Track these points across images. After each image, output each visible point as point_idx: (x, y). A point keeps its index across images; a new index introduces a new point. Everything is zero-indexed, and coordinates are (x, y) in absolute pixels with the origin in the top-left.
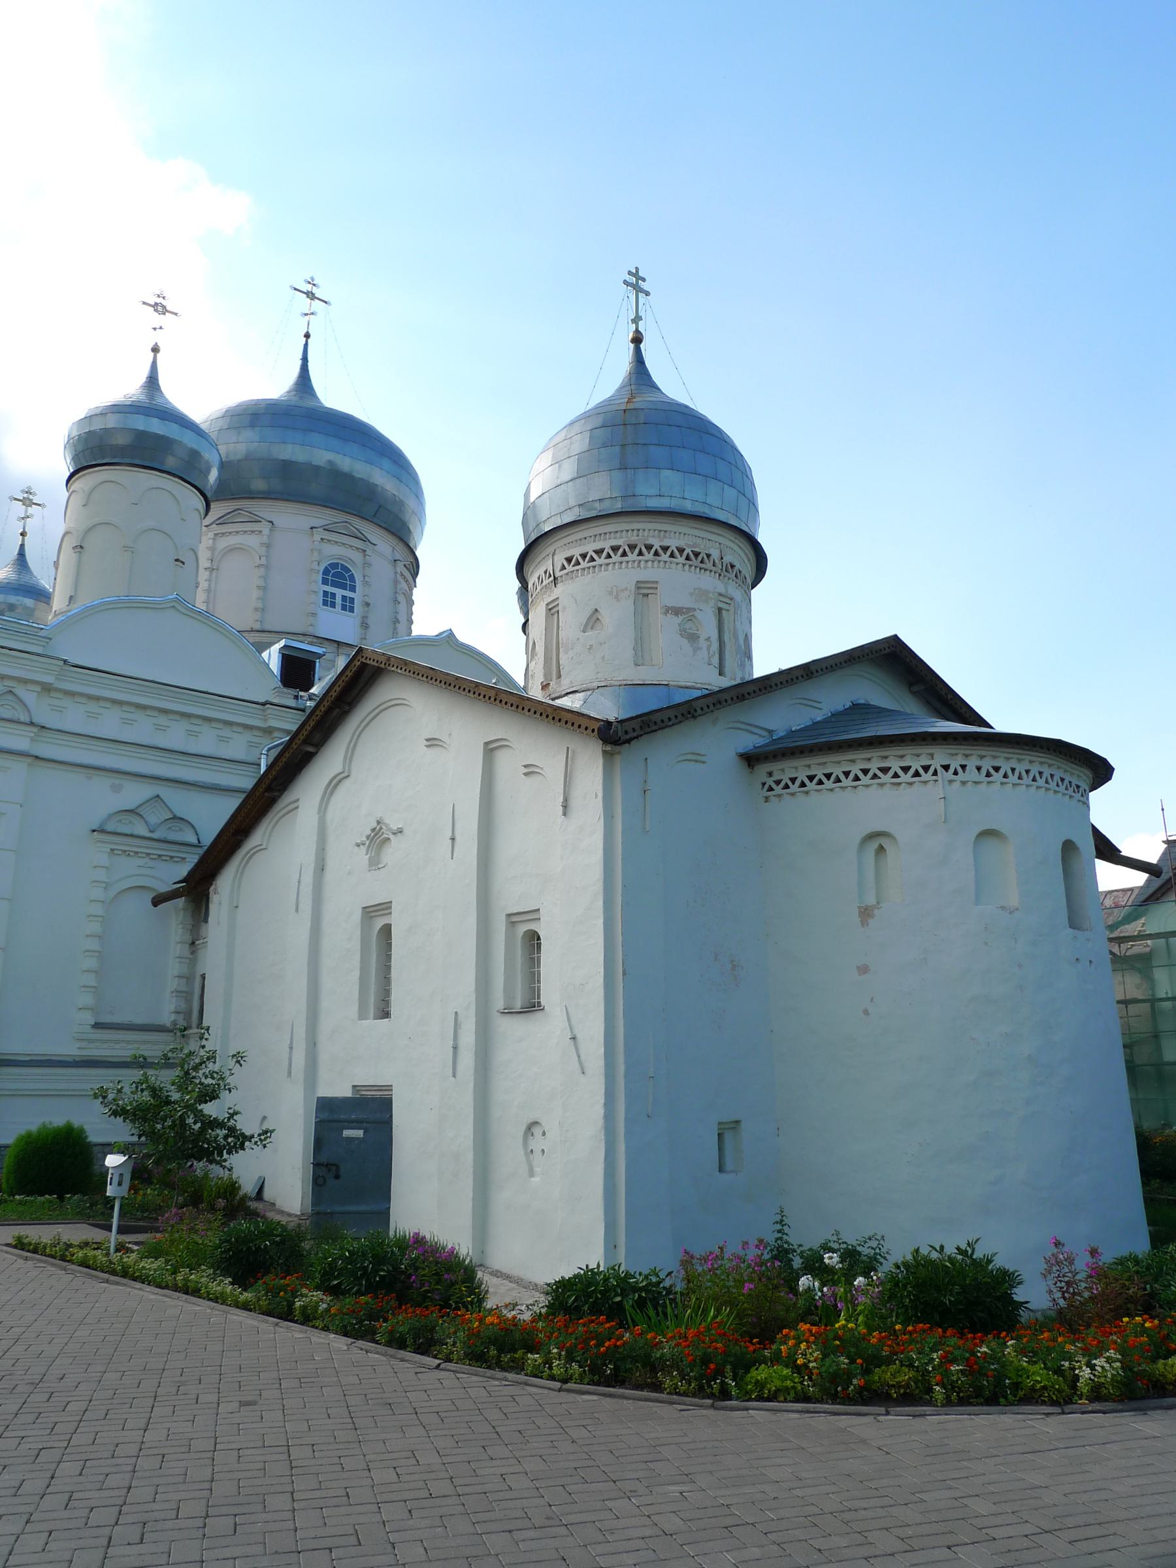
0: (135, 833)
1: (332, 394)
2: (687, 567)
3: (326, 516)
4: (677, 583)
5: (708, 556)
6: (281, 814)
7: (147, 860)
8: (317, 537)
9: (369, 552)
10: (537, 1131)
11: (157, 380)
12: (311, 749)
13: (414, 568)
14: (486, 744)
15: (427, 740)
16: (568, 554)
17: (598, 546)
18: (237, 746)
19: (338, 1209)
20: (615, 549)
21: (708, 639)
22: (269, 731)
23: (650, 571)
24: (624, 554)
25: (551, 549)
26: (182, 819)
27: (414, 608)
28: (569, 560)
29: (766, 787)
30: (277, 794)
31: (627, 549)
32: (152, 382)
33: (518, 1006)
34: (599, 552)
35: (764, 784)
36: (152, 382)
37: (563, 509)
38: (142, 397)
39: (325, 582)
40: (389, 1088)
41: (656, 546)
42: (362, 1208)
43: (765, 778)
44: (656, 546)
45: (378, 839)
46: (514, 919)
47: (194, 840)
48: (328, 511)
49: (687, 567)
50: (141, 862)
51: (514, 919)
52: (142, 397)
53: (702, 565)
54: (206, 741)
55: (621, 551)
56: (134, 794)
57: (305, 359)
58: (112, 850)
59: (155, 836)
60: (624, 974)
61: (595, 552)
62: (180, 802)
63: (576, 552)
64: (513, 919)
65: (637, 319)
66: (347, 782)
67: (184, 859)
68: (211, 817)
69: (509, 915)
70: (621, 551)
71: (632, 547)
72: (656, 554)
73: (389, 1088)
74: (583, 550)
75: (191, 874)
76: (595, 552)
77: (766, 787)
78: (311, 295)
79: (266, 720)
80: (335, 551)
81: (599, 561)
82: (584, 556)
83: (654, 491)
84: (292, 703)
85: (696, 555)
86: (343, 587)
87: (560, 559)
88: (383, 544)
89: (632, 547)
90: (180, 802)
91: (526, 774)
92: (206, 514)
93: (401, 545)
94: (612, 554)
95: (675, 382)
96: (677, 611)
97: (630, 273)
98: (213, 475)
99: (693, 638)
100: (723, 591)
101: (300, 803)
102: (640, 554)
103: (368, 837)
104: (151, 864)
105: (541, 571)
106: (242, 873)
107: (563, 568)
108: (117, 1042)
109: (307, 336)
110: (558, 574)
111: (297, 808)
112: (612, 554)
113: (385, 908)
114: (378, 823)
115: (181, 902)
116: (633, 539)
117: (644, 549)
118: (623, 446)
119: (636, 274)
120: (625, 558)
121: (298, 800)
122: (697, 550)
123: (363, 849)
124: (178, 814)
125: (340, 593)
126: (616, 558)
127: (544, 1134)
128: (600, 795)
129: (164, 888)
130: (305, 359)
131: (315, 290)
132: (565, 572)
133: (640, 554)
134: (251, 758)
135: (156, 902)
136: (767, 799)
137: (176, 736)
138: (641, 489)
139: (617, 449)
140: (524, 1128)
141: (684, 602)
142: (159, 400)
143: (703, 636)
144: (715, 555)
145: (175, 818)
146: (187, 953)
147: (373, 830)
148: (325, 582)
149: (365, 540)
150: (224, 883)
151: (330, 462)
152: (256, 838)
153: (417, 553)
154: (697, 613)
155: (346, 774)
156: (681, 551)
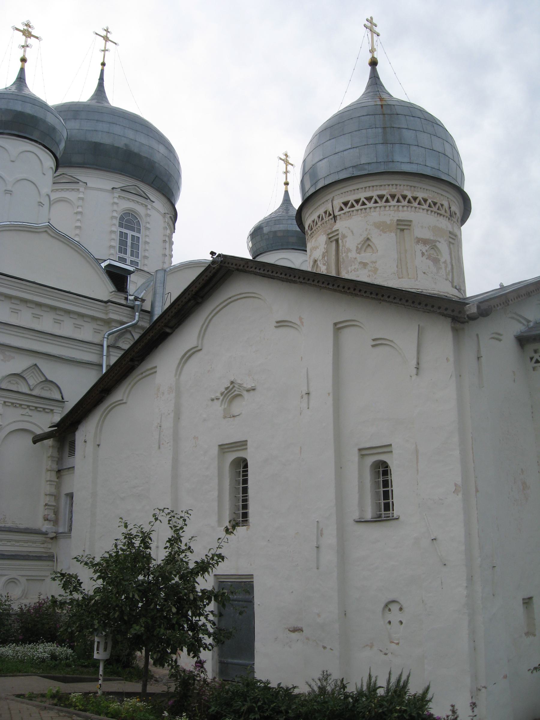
0: (20, 390)
1: (116, 99)
2: (429, 212)
3: (120, 181)
4: (423, 221)
5: (442, 205)
6: (138, 378)
7: (28, 410)
8: (116, 195)
9: (149, 207)
10: (394, 608)
11: (24, 80)
12: (168, 330)
13: (174, 217)
14: (335, 324)
15: (277, 322)
16: (345, 200)
17: (368, 194)
18: (87, 333)
19: (230, 660)
20: (381, 197)
21: (445, 262)
22: (108, 322)
23: (406, 214)
24: (387, 201)
25: (330, 196)
26: (52, 382)
27: (173, 247)
28: (346, 204)
29: (534, 360)
30: (136, 363)
31: (389, 197)
32: (21, 79)
33: (369, 516)
34: (369, 199)
35: (531, 359)
36: (21, 79)
37: (340, 169)
38: (13, 89)
39: (121, 225)
40: (251, 576)
41: (409, 196)
42: (236, 661)
43: (532, 354)
44: (409, 196)
45: (232, 393)
46: (364, 452)
47: (59, 398)
48: (122, 177)
49: (429, 212)
50: (24, 412)
51: (364, 452)
52: (13, 89)
53: (439, 211)
54: (67, 328)
55: (385, 199)
56: (19, 364)
57: (101, 79)
58: (5, 402)
59: (34, 393)
60: (477, 491)
61: (366, 198)
62: (52, 371)
63: (351, 198)
64: (363, 452)
65: (372, 51)
66: (199, 355)
67: (52, 410)
68: (75, 386)
69: (360, 450)
70: (385, 199)
71: (393, 196)
72: (409, 202)
73: (251, 576)
74: (357, 197)
75: (63, 420)
76: (366, 198)
77: (534, 360)
78: (106, 39)
79: (107, 314)
80: (125, 205)
81: (369, 205)
82: (357, 201)
83: (406, 160)
84: (123, 302)
85: (435, 204)
86: (133, 229)
87: (338, 202)
88: (159, 203)
89: (393, 196)
90: (52, 371)
91: (373, 346)
92: (55, 172)
93: (169, 203)
94: (378, 200)
95: (401, 86)
96: (425, 242)
97: (367, 20)
98: (62, 146)
99: (436, 261)
100: (451, 230)
101: (158, 369)
102: (398, 201)
103: (222, 394)
104: (30, 413)
105: (321, 211)
106: (105, 418)
107: (341, 209)
108: (9, 541)
109: (103, 64)
110: (337, 213)
111: (156, 372)
112: (378, 200)
113: (242, 445)
114: (232, 383)
115: (49, 442)
116: (394, 191)
117: (401, 198)
118: (384, 128)
119: (370, 20)
120: (389, 204)
121: (156, 367)
122: (435, 201)
123: (217, 403)
124: (49, 378)
125: (130, 233)
126: (382, 203)
127: (401, 609)
128: (452, 359)
129: (39, 432)
130: (101, 79)
131: (109, 35)
132: (343, 212)
133: (398, 201)
134: (96, 340)
135: (37, 439)
136: (534, 369)
137: (47, 323)
138: (398, 158)
139: (380, 130)
140: (383, 605)
141: (427, 235)
142: (25, 92)
143: (442, 260)
144: (446, 204)
145: (47, 380)
146: (54, 478)
147: (227, 388)
148: (121, 225)
149: (147, 198)
150: (85, 434)
151: (126, 145)
152: (118, 395)
153: (177, 206)
154: (437, 244)
155: (199, 348)
156: (425, 201)
